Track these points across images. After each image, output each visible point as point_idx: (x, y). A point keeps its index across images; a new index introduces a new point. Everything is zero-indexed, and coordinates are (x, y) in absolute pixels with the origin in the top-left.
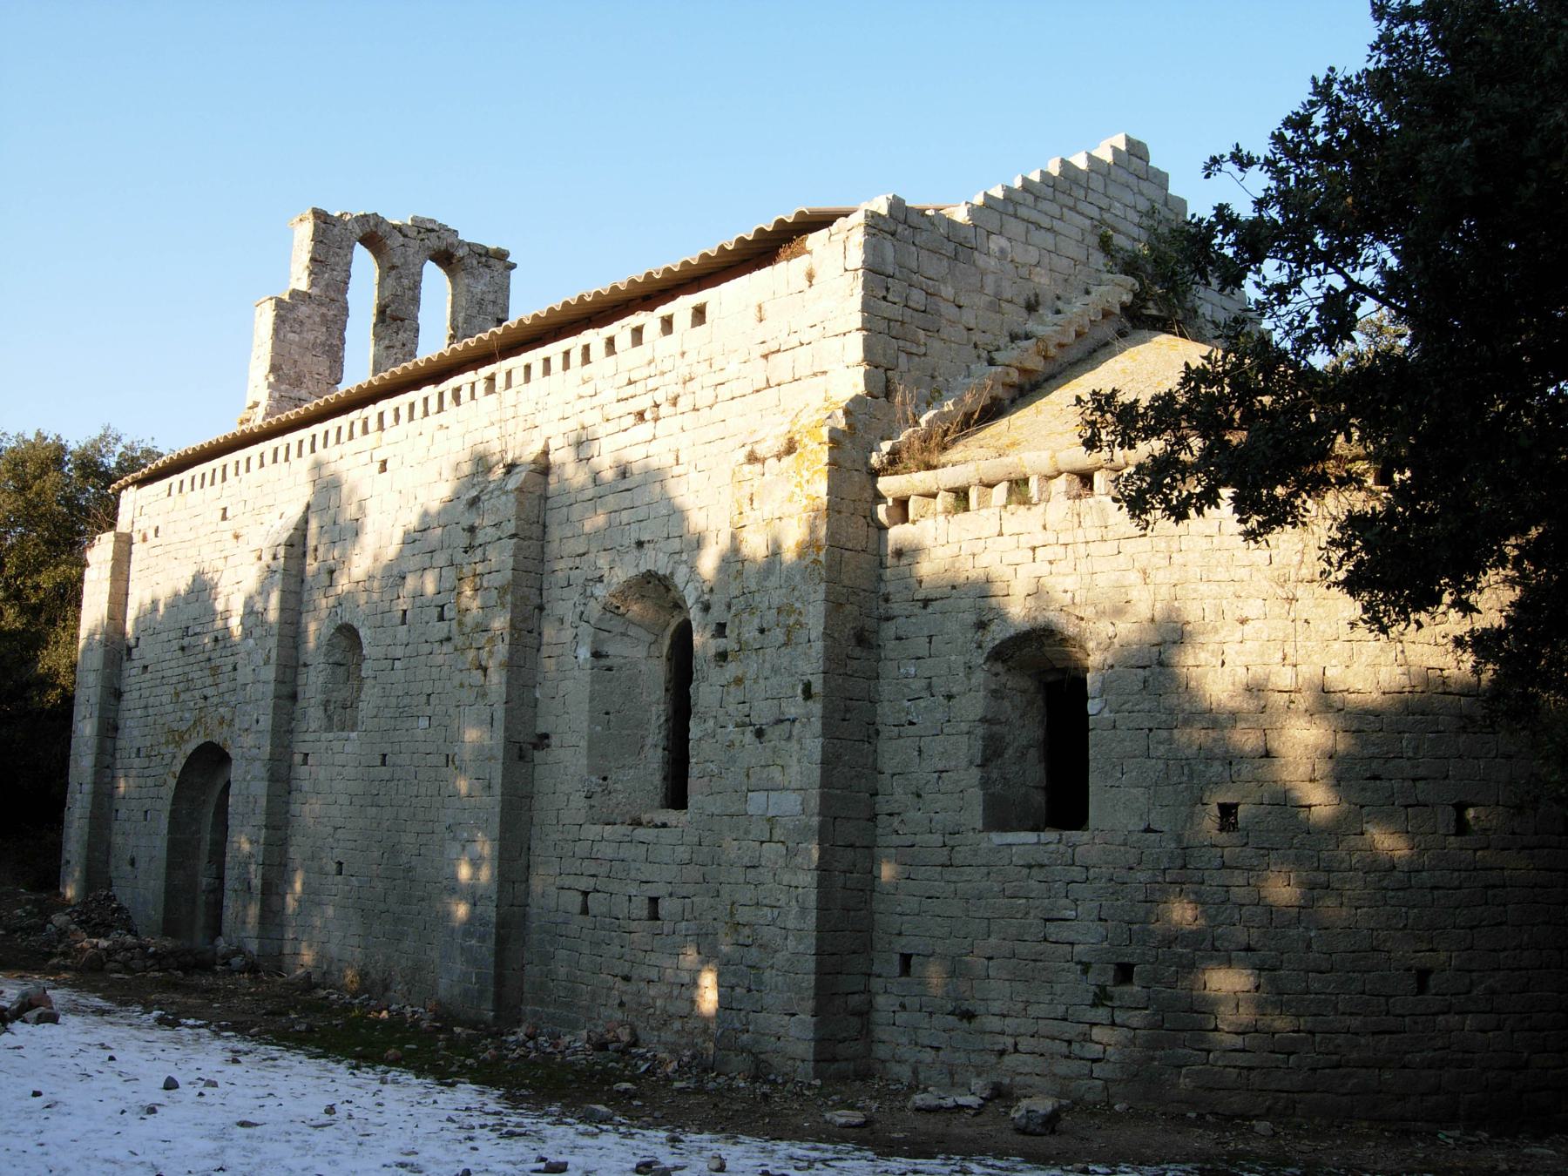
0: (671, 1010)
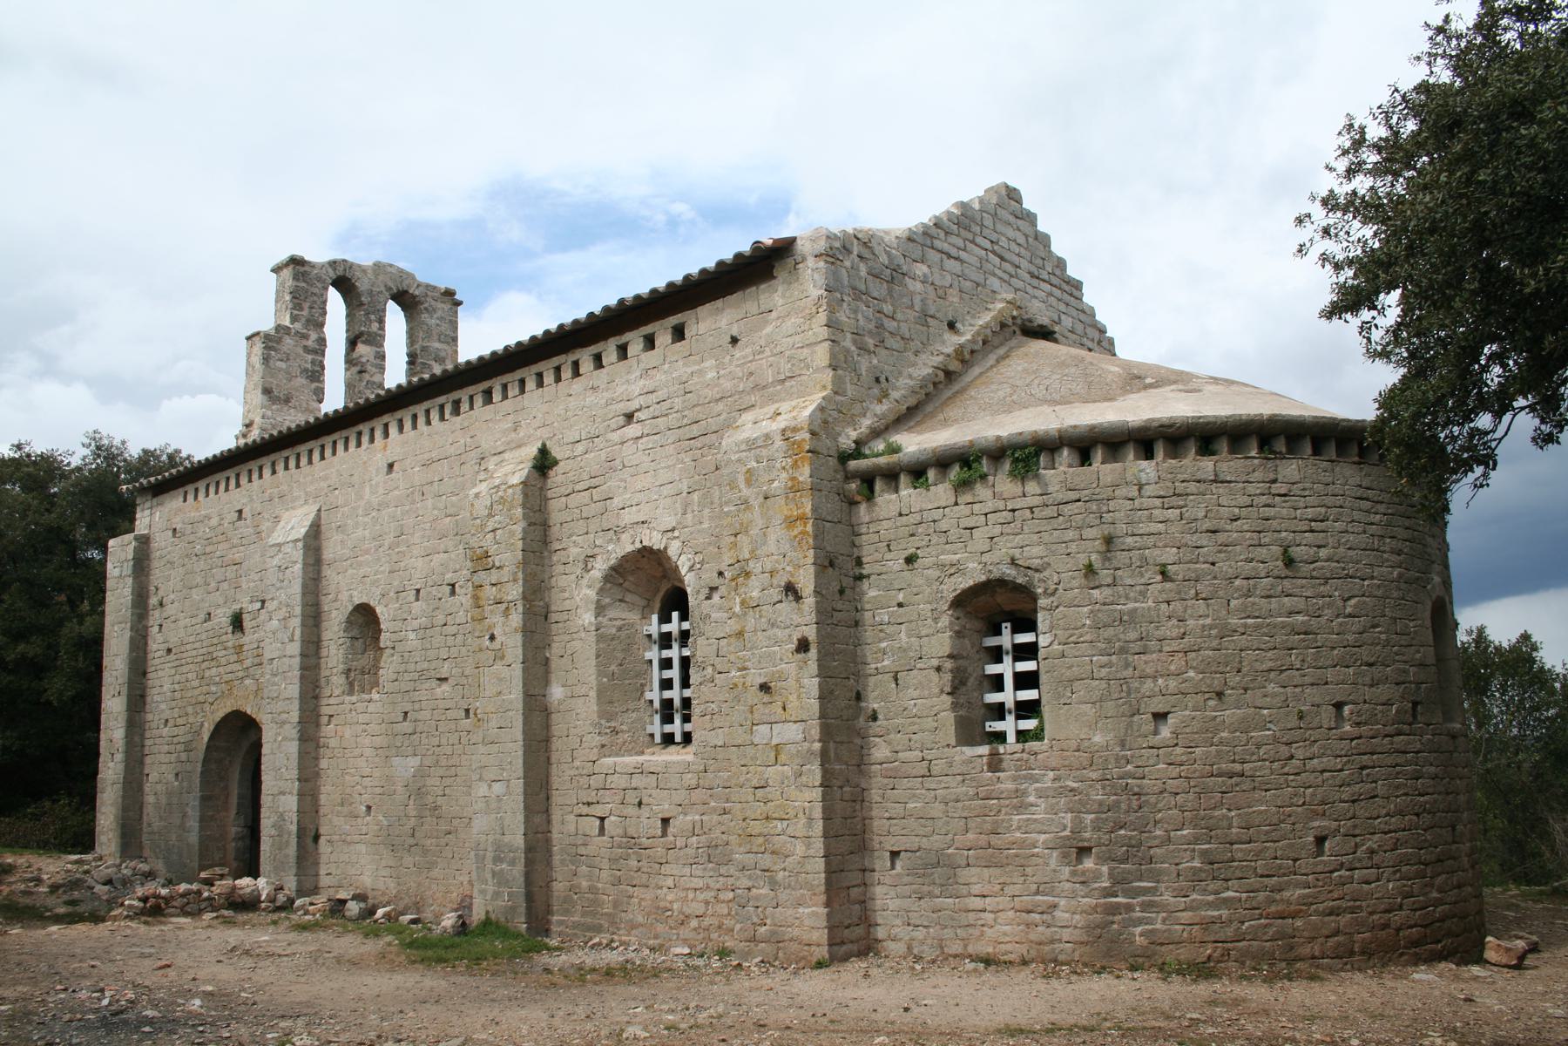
0: (688, 911)
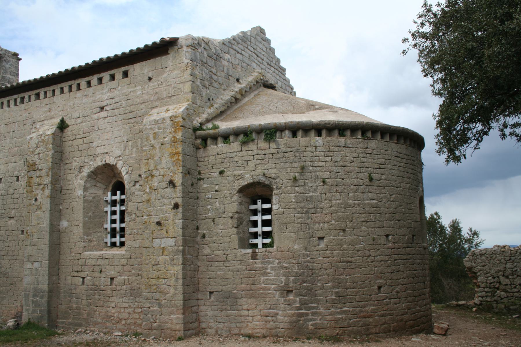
0: (121, 317)
